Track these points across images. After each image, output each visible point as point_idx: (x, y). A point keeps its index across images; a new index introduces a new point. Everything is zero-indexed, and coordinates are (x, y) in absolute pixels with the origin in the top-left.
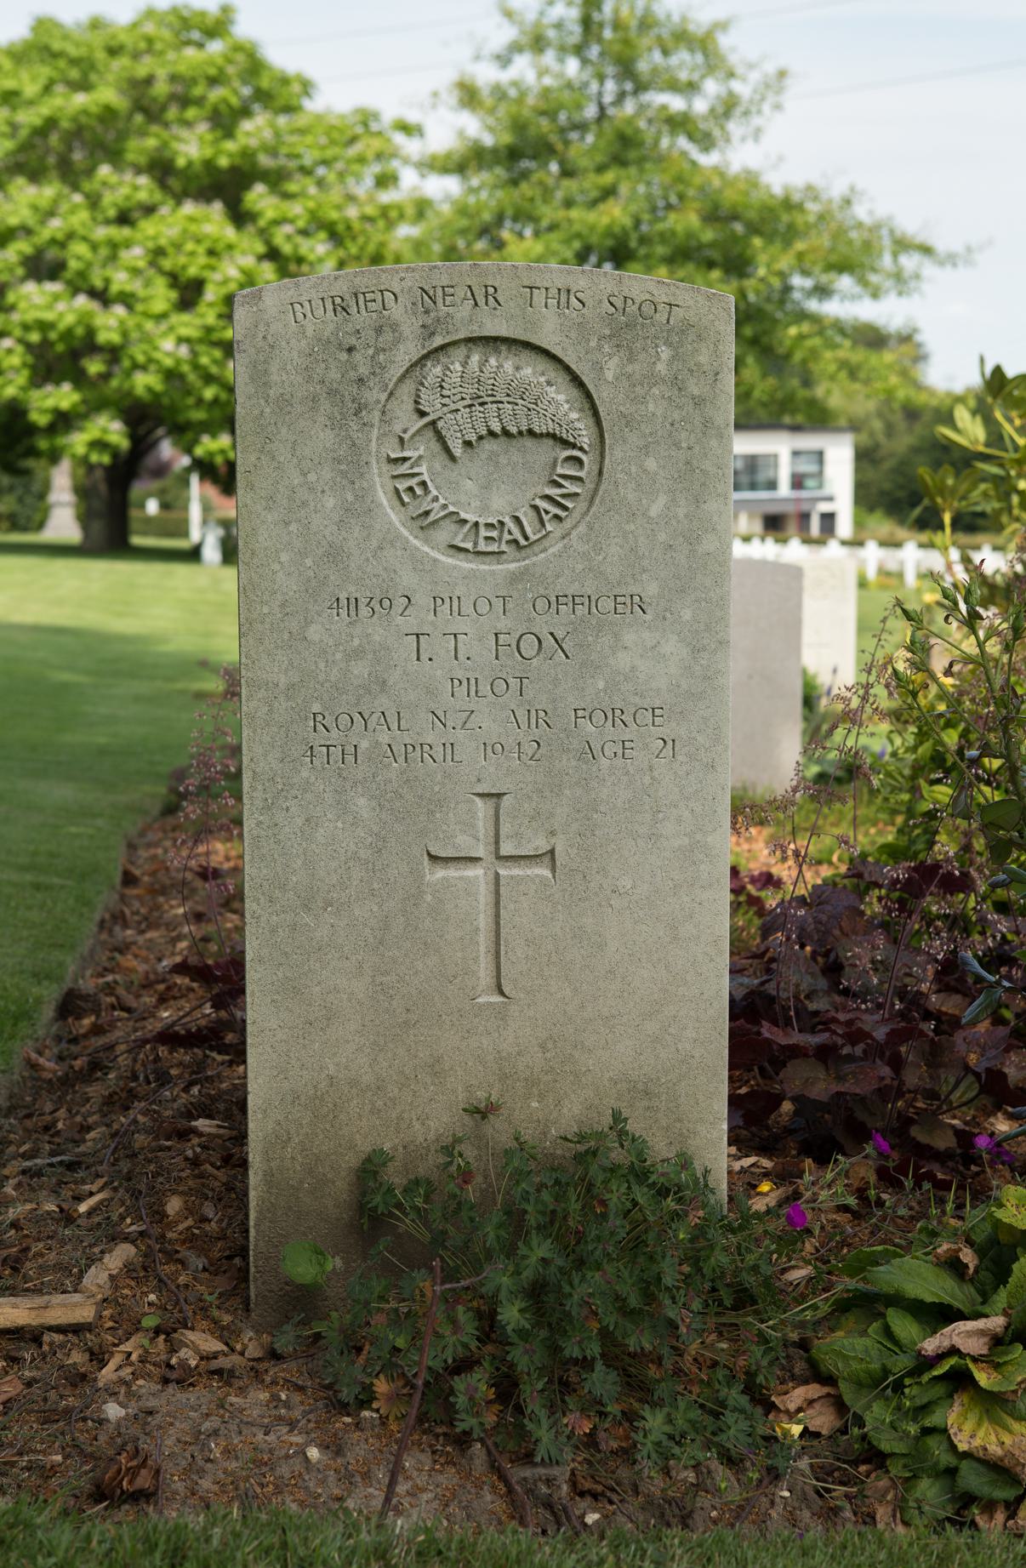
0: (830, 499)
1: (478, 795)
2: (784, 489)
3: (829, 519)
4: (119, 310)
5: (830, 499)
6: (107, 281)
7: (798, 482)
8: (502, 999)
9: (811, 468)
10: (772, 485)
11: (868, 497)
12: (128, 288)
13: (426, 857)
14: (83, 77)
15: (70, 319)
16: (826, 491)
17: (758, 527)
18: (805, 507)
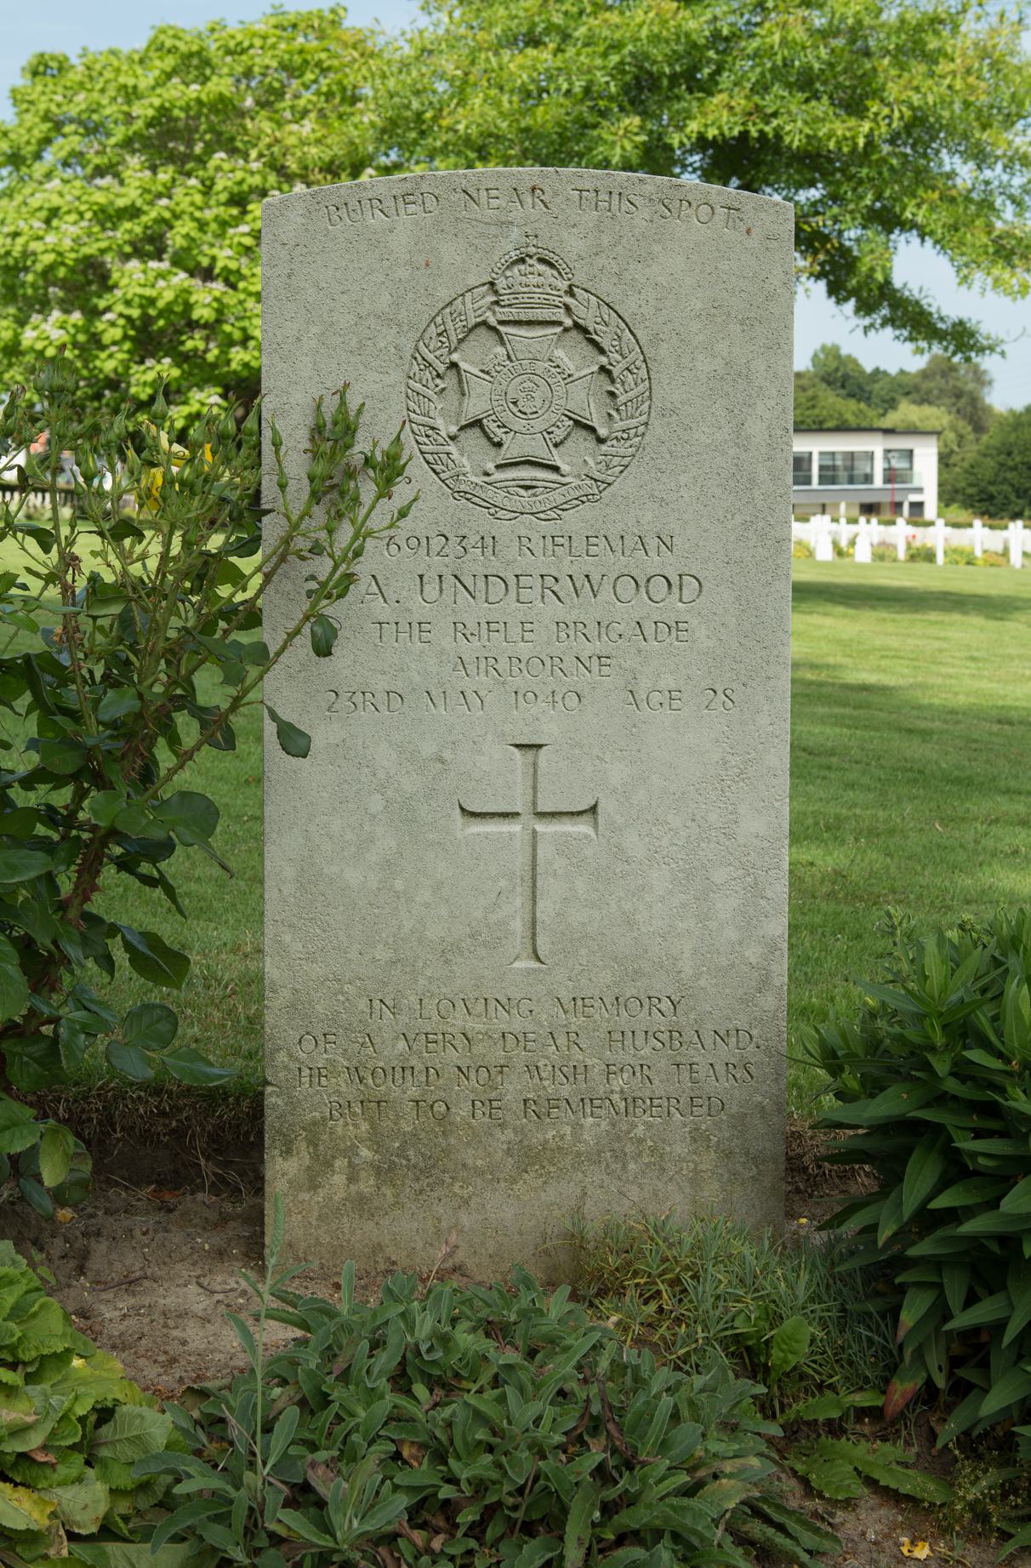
0: (920, 490)
1: (517, 746)
2: (878, 481)
3: (917, 507)
4: (218, 287)
5: (920, 490)
6: (214, 259)
7: (891, 476)
8: (538, 965)
9: (903, 465)
10: (868, 479)
11: (948, 496)
12: (233, 265)
13: (458, 811)
14: (195, 64)
15: (169, 296)
16: (916, 483)
17: (856, 512)
18: (897, 499)
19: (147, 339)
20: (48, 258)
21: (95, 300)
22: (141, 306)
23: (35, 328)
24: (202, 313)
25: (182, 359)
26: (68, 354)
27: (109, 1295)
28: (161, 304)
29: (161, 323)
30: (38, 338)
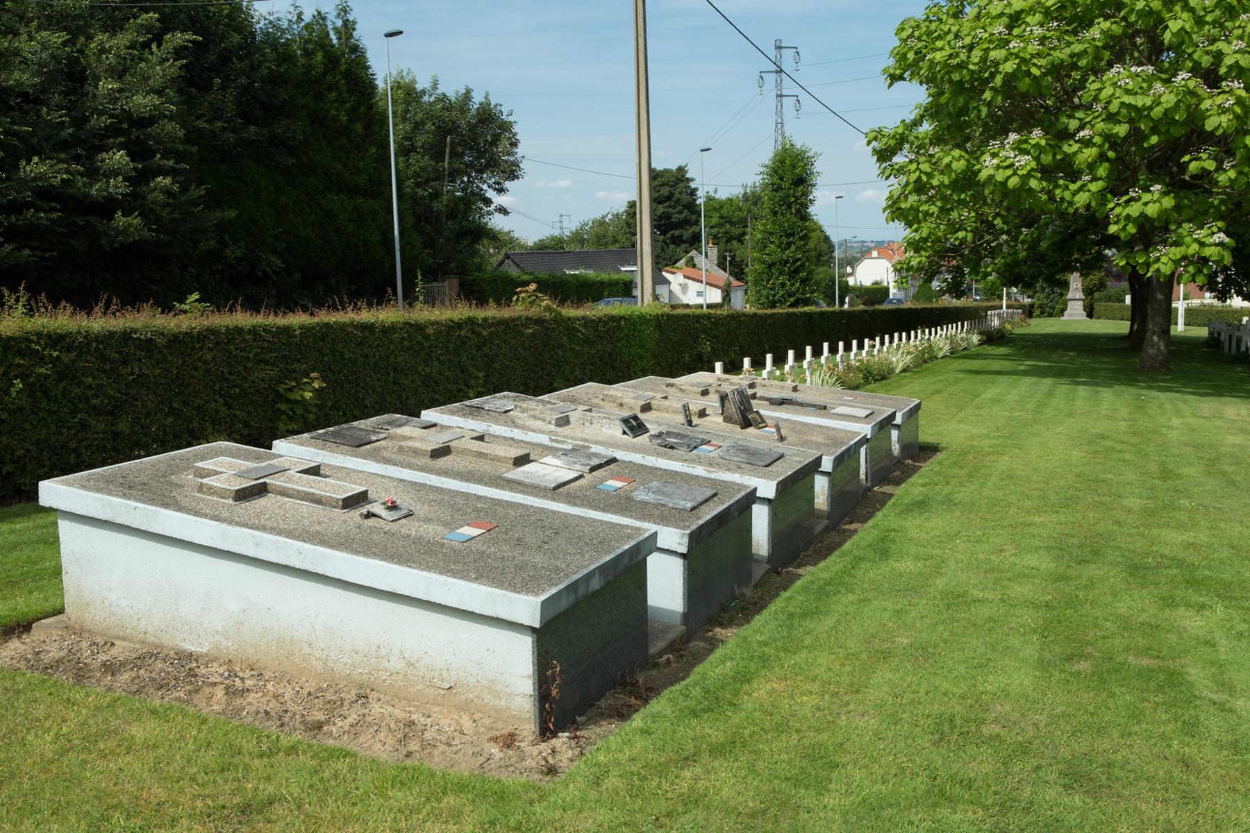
15: (1169, 99)
19: (1128, 165)
20: (1009, 67)
21: (1064, 120)
22: (1131, 121)
23: (994, 155)
24: (1217, 122)
25: (1178, 184)
26: (1033, 184)
27: (1143, 617)
28: (1157, 112)
29: (1154, 140)
30: (998, 167)
